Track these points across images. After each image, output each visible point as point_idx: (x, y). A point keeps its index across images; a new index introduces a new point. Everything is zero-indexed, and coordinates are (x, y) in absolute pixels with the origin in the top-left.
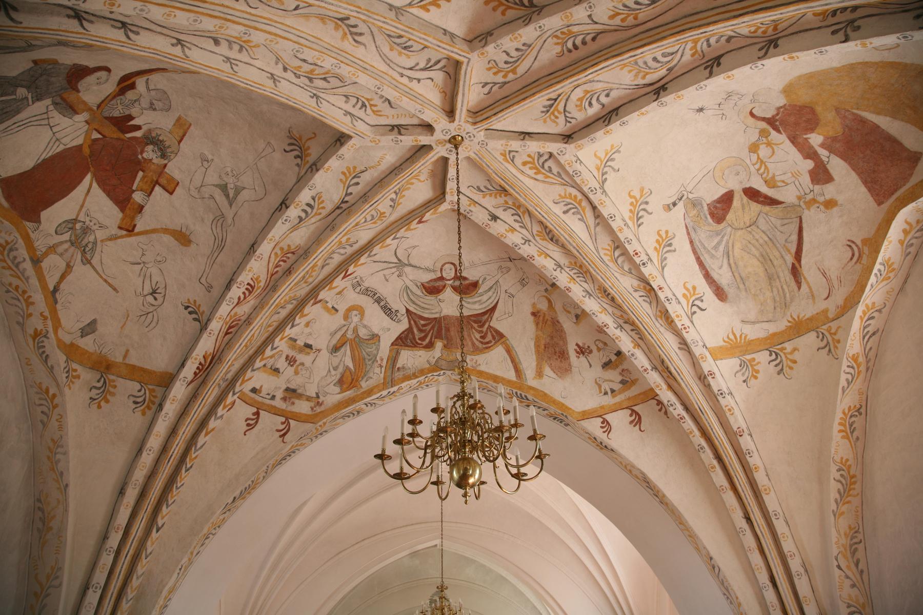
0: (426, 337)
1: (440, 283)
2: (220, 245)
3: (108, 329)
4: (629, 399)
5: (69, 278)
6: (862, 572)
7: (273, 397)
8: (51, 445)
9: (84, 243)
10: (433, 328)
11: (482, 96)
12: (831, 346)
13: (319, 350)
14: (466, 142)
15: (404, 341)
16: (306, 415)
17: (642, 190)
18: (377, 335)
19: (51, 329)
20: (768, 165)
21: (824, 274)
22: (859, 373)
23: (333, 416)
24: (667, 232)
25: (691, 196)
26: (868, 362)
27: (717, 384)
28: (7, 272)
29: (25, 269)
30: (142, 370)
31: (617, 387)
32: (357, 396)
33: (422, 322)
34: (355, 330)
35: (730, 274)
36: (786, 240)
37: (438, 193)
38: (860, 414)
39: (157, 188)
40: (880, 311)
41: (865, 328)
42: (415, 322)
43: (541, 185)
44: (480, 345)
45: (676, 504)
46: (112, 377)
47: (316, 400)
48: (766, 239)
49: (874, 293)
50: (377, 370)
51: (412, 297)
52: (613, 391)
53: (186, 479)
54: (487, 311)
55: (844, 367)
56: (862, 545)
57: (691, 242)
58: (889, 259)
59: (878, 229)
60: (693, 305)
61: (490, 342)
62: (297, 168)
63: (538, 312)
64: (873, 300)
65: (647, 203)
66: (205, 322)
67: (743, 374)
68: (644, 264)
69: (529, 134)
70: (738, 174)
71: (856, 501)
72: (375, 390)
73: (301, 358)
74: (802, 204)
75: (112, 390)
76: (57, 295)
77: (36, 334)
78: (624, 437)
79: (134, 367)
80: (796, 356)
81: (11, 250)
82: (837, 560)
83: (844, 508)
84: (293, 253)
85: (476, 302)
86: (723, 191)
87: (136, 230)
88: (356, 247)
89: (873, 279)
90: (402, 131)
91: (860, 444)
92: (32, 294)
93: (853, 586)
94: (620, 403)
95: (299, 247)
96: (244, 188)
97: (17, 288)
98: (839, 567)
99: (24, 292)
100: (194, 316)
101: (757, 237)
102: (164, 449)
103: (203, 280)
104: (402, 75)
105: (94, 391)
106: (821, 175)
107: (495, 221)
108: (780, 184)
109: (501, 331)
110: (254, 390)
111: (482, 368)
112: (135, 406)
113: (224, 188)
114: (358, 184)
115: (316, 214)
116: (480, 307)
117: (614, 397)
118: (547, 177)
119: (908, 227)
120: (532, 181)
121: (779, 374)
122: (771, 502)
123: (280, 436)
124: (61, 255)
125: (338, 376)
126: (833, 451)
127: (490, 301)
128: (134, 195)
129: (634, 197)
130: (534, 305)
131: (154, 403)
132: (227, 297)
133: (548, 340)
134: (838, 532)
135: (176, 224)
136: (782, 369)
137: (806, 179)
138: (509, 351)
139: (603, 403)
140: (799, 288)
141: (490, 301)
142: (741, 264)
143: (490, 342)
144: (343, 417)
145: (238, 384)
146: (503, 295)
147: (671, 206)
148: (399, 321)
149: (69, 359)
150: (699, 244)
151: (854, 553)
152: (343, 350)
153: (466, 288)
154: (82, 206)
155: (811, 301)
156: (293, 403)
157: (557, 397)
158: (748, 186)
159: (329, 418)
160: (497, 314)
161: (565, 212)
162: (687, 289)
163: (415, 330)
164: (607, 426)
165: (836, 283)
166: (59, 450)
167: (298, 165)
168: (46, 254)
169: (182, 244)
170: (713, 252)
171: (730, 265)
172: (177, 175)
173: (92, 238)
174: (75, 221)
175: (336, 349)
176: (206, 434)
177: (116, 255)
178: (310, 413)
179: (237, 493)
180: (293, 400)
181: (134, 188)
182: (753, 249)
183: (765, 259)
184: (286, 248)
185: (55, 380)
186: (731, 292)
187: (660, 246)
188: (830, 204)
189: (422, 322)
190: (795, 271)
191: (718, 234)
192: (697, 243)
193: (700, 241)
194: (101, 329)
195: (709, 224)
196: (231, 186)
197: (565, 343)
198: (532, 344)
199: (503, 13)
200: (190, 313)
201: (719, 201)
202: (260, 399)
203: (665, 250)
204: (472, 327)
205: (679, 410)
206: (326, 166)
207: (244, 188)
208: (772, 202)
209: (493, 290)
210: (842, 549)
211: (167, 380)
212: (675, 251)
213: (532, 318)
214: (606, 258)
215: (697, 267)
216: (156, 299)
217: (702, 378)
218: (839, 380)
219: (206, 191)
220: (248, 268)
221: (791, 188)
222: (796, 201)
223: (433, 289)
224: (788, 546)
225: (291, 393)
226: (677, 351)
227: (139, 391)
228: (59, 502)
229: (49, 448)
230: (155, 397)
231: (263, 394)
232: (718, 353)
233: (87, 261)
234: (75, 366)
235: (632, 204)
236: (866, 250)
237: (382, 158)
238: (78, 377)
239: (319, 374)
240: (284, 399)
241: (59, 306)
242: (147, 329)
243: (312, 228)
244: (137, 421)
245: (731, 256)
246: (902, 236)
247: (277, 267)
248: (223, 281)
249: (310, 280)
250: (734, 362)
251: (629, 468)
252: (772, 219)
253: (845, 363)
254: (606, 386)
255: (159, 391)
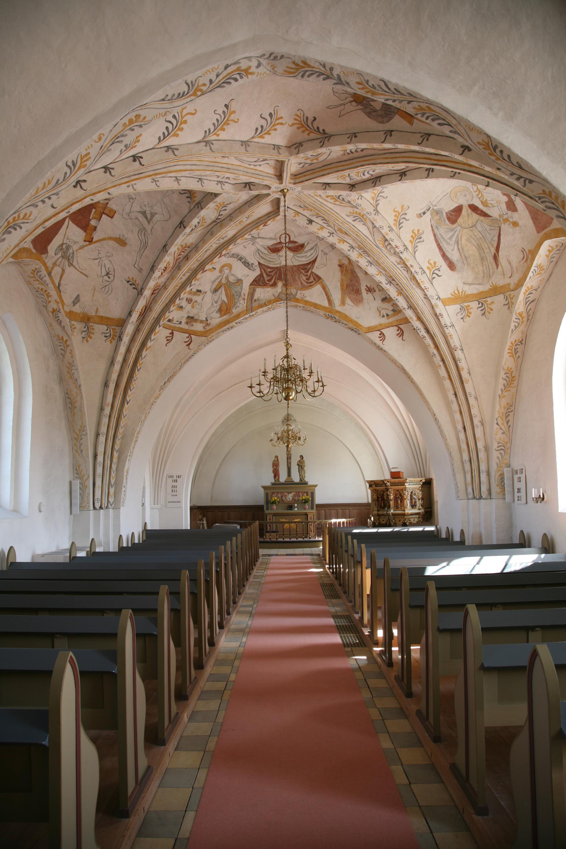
0: (271, 279)
1: (280, 246)
2: (145, 246)
3: (86, 299)
4: (397, 320)
5: (64, 276)
6: (510, 426)
7: (180, 323)
8: (68, 365)
9: (68, 255)
10: (276, 273)
11: (299, 168)
12: (510, 304)
13: (206, 292)
14: (290, 191)
15: (258, 282)
16: (200, 331)
17: (403, 207)
18: (241, 280)
19: (61, 308)
20: (484, 194)
21: (510, 263)
22: (522, 322)
23: (217, 332)
24: (418, 230)
25: (435, 208)
26: (528, 316)
27: (445, 320)
28: (37, 282)
29: (45, 281)
30: (108, 318)
31: (390, 313)
32: (231, 318)
33: (269, 270)
34: (227, 278)
35: (459, 254)
36: (492, 239)
37: (275, 208)
38: (522, 344)
39: (104, 216)
40: (536, 290)
41: (527, 298)
42: (264, 270)
43: (338, 207)
44: (306, 284)
45: (418, 384)
46: (91, 324)
47: (206, 322)
48: (481, 236)
49: (532, 281)
50: (242, 302)
51: (262, 255)
52: (387, 315)
53: (138, 375)
54: (310, 262)
55: (514, 319)
56: (512, 413)
57: (435, 235)
58: (540, 264)
59: (536, 247)
60: (433, 273)
61: (312, 282)
62: (188, 204)
63: (343, 265)
64: (531, 284)
65: (406, 214)
66: (140, 289)
67: (462, 314)
68: (401, 253)
69: (328, 184)
70: (465, 196)
71: (513, 390)
72: (242, 315)
73: (195, 298)
74: (501, 220)
75: (92, 331)
76: (61, 288)
77: (54, 311)
78: (393, 344)
79: (102, 317)
80: (493, 306)
81: (38, 272)
82: (497, 420)
83: (506, 394)
84: (189, 247)
85: (303, 257)
86: (455, 205)
87: (94, 240)
88: (226, 239)
89: (530, 274)
90: (252, 187)
91: (520, 360)
92: (50, 292)
93: (503, 433)
94: (391, 323)
95: (192, 244)
96: (156, 214)
97: (42, 289)
98: (497, 424)
99: (46, 291)
100: (133, 286)
101: (476, 234)
102: (125, 360)
103: (136, 266)
104: (250, 165)
105: (84, 333)
106: (511, 206)
107: (311, 223)
108: (489, 205)
109: (319, 275)
110: (169, 321)
111: (307, 299)
112: (105, 338)
113: (144, 213)
114: (226, 210)
115: (201, 226)
116: (306, 260)
117: (388, 319)
118: (342, 203)
119: (551, 249)
120: (332, 205)
121: (482, 315)
122: (469, 388)
123: (187, 345)
124: (59, 266)
125: (218, 307)
126: (503, 363)
127: (312, 256)
128: (91, 222)
129: (398, 212)
130: (340, 260)
131: (116, 336)
132: (153, 277)
133: (348, 282)
134: (500, 406)
135: (117, 234)
136: (484, 313)
137: (504, 207)
138: (324, 288)
139: (382, 322)
140: (497, 268)
141: (312, 256)
142: (465, 249)
143: (312, 282)
144: (223, 331)
145: (161, 321)
146: (320, 253)
147: (422, 214)
148: (254, 270)
149: (71, 320)
150: (439, 237)
151: (507, 417)
152: (220, 290)
153: (298, 248)
154: (65, 235)
155: (502, 277)
156: (192, 325)
157: (353, 317)
158: (471, 203)
159: (215, 333)
160: (316, 264)
161: (353, 221)
162: (430, 264)
163: (265, 275)
164: (382, 336)
165: (515, 270)
166: (73, 368)
167: (189, 202)
168: (53, 268)
169: (121, 245)
170: (448, 241)
171: (458, 249)
172: (114, 207)
173: (71, 251)
174: (63, 244)
175: (216, 290)
176: (147, 350)
177: (85, 257)
178: (203, 330)
179: (166, 380)
180: (192, 323)
181: (91, 218)
182: (473, 241)
183: (480, 248)
184: (184, 245)
185: (66, 333)
186: (458, 265)
187: (414, 239)
188: (515, 224)
189: (269, 270)
190: (496, 258)
191: (452, 230)
192: (438, 236)
193: (440, 235)
194: (82, 299)
195: (447, 225)
196: (148, 212)
197: (359, 285)
198: (339, 284)
199: (308, 134)
200: (131, 285)
201: (453, 211)
202: (173, 325)
203: (417, 241)
204: (301, 272)
205: (423, 332)
206: (207, 207)
207: (156, 214)
208: (485, 215)
209: (314, 250)
210: (501, 415)
211: (122, 323)
212: (423, 241)
213: (339, 268)
214: (380, 246)
215: (438, 250)
216: (109, 278)
217: (437, 316)
218: (510, 326)
219: (133, 215)
220: (164, 260)
221: (496, 209)
222: (498, 217)
223: (275, 249)
224: (474, 411)
225: (191, 319)
226: (423, 299)
227: (107, 330)
228: (77, 394)
229: (68, 368)
230: (116, 332)
231: (174, 322)
232: (446, 302)
233: (71, 264)
234: (73, 322)
235: (395, 216)
236: (530, 256)
237: (240, 198)
238: (75, 328)
239: (207, 307)
240: (187, 323)
241: (62, 294)
242: (106, 295)
243: (199, 233)
244: (108, 347)
245: (460, 244)
246: (547, 253)
247: (179, 255)
248: (148, 266)
249: (199, 259)
250: (457, 307)
251: (394, 362)
252: (485, 225)
253: (514, 317)
254: (384, 312)
255: (118, 329)
